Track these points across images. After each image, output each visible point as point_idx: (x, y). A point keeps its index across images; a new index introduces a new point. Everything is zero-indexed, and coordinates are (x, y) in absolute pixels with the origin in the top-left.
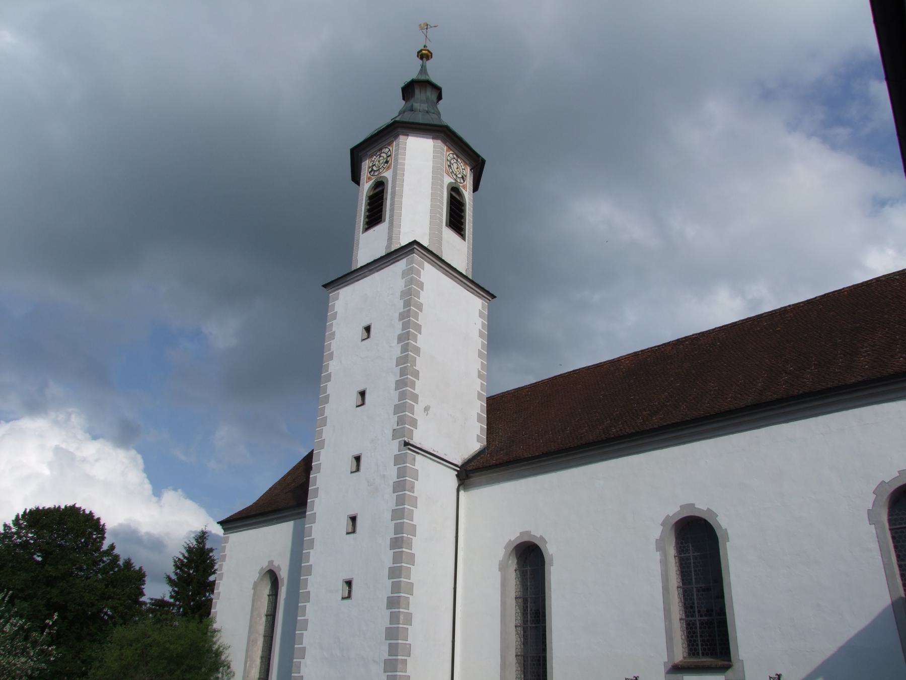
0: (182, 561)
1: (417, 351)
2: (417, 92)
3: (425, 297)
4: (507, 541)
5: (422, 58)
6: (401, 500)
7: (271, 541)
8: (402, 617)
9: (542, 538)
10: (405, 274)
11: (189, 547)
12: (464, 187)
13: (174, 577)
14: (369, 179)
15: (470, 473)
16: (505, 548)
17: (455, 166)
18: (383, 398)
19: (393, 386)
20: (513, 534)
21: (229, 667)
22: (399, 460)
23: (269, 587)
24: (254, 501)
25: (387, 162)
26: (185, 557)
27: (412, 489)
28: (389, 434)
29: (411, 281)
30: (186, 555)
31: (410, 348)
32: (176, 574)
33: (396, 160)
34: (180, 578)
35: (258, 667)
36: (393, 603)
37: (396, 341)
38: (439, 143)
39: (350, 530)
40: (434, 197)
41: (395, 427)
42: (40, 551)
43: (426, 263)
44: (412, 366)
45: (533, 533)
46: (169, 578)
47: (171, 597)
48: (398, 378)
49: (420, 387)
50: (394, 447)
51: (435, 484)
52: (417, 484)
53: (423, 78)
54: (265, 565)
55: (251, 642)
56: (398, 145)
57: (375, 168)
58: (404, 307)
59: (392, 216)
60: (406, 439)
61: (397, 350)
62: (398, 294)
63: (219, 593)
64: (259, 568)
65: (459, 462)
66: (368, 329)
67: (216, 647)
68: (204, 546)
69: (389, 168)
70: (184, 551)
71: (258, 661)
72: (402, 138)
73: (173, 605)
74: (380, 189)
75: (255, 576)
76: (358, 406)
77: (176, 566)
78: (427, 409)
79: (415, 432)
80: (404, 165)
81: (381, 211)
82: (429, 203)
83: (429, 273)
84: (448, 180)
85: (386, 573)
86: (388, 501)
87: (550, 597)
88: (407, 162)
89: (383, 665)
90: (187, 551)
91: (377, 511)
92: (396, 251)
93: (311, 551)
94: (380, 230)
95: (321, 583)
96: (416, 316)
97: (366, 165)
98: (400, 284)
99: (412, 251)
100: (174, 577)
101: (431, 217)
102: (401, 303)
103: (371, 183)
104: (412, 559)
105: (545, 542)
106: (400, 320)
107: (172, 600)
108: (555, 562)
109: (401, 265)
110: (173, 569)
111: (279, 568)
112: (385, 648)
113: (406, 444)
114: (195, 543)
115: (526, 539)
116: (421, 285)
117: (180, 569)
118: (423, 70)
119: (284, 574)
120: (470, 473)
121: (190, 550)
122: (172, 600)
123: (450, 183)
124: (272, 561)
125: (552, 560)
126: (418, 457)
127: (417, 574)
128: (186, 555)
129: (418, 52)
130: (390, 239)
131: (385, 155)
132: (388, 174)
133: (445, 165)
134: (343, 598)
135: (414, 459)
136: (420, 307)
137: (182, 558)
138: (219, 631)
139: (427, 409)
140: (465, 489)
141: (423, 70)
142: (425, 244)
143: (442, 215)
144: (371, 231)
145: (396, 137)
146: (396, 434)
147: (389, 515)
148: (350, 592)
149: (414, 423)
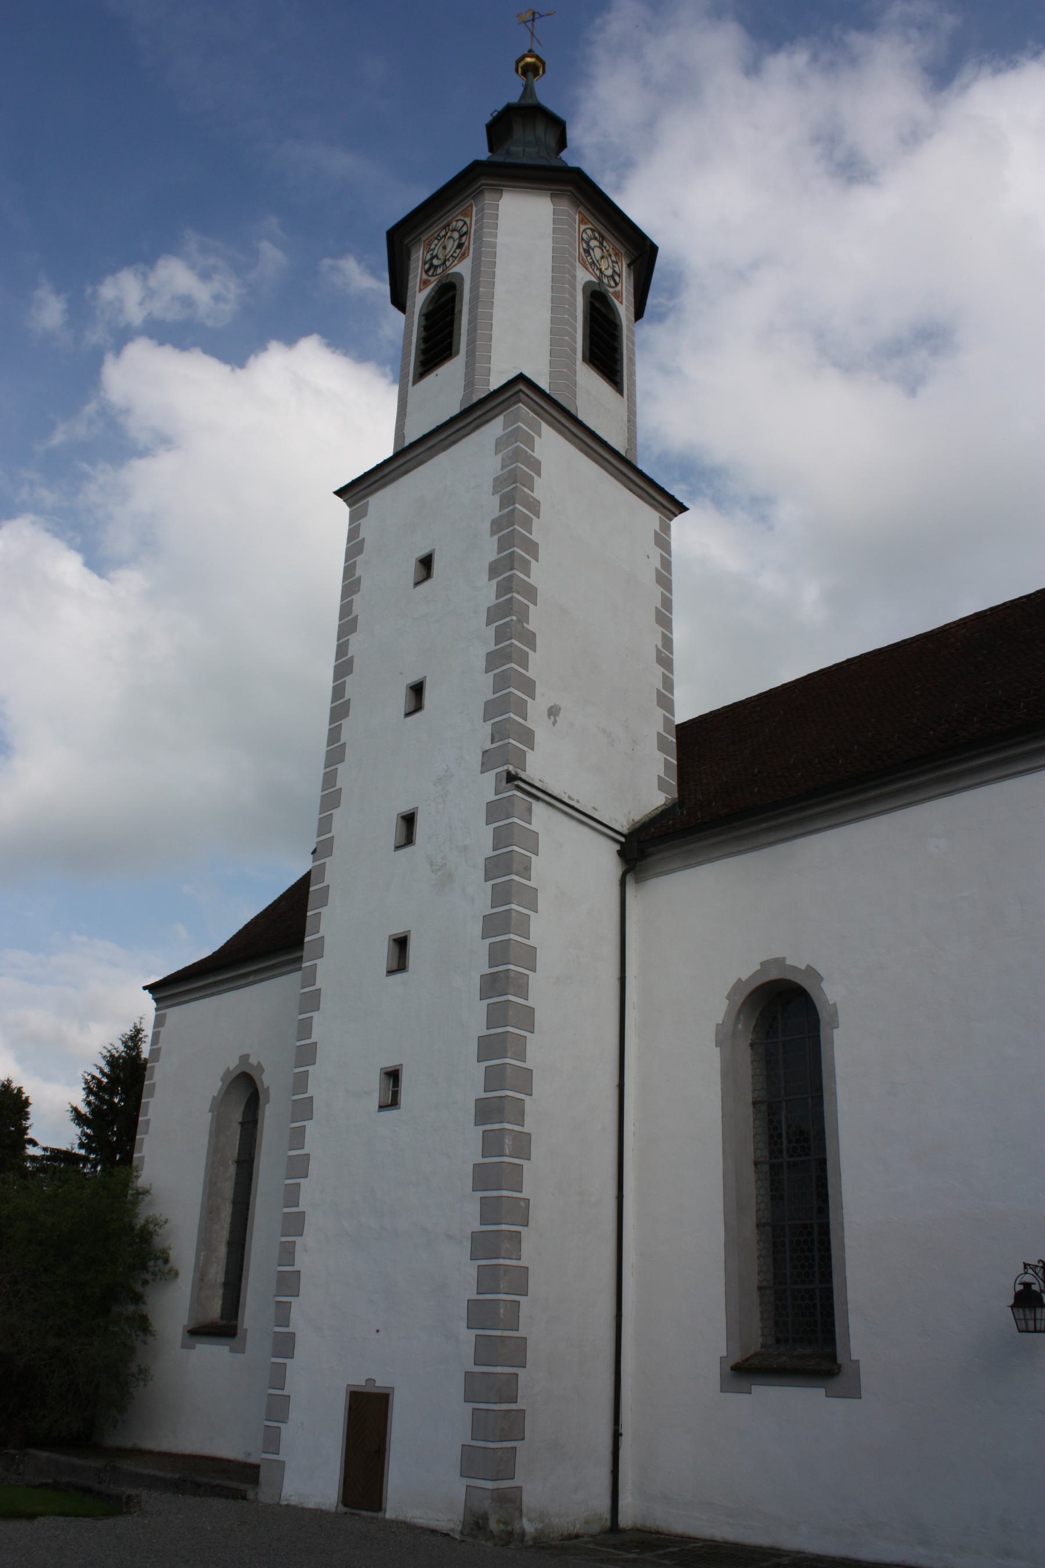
0: (99, 1082)
1: (531, 593)
2: (517, 129)
3: (542, 490)
4: (732, 981)
5: (524, 73)
6: (501, 895)
7: (242, 1019)
8: (508, 1141)
9: (810, 971)
10: (500, 444)
11: (112, 1056)
12: (618, 295)
13: (84, 1109)
14: (425, 283)
15: (643, 849)
16: (728, 997)
17: (597, 253)
18: (461, 691)
19: (482, 663)
20: (744, 966)
21: (166, 1261)
22: (495, 811)
23: (241, 1109)
24: (216, 948)
25: (460, 246)
26: (102, 1072)
27: (526, 871)
28: (476, 760)
29: (517, 455)
30: (107, 1070)
31: (516, 565)
32: (89, 1104)
33: (479, 237)
34: (95, 1110)
35: (223, 1262)
36: (493, 985)
37: (486, 577)
38: (565, 206)
39: (395, 967)
40: (558, 305)
41: (488, 746)
42: (24, 1173)
43: (544, 426)
44: (519, 621)
45: (788, 962)
46: (75, 1110)
47: (82, 1145)
48: (492, 647)
49: (538, 665)
50: (487, 787)
51: (573, 867)
52: (537, 863)
53: (529, 101)
54: (233, 1063)
55: (209, 1213)
56: (481, 211)
57: (435, 262)
58: (502, 506)
59: (472, 342)
60: (511, 768)
61: (487, 593)
62: (488, 485)
63: (148, 1122)
64: (221, 1072)
65: (623, 824)
66: (426, 563)
67: (140, 1222)
68: (138, 1055)
69: (463, 256)
70: (102, 1064)
71: (222, 1251)
72: (488, 198)
73: (85, 1159)
74: (450, 294)
75: (214, 1087)
76: (407, 715)
77: (89, 1090)
78: (553, 712)
79: (530, 756)
80: (494, 245)
81: (450, 335)
82: (547, 315)
83: (551, 446)
84: (584, 276)
85: (472, 1048)
86: (475, 897)
87: (834, 1094)
88: (500, 240)
89: (468, 1244)
90: (108, 1063)
91: (452, 924)
92: (481, 402)
93: (315, 1014)
94: (451, 371)
95: (340, 1084)
96: (527, 524)
97: (418, 258)
98: (492, 465)
99: (515, 398)
100: (84, 1109)
101: (553, 342)
102: (496, 500)
103: (427, 291)
104: (527, 1018)
105: (819, 978)
106: (493, 533)
107: (83, 1152)
108: (841, 1019)
109: (495, 428)
110: (82, 1095)
111: (260, 1068)
112: (473, 1209)
113: (511, 778)
114: (122, 1048)
115: (774, 975)
116: (536, 466)
117: (95, 1094)
118: (528, 90)
119: (274, 1082)
120: (643, 849)
121: (112, 1061)
122: (83, 1152)
123: (587, 285)
124: (248, 1055)
125: (835, 1014)
126: (538, 808)
127: (539, 1051)
128: (107, 1070)
129: (518, 62)
130: (469, 384)
131: (456, 235)
132: (463, 268)
133: (578, 249)
134: (382, 1107)
135: (530, 810)
136: (534, 507)
137: (99, 1076)
138: (146, 1192)
139: (553, 712)
140: (638, 881)
141: (528, 90)
142: (544, 384)
143: (574, 305)
144: (431, 378)
145: (478, 194)
146: (488, 761)
147: (477, 928)
148: (395, 1095)
149: (528, 737)
